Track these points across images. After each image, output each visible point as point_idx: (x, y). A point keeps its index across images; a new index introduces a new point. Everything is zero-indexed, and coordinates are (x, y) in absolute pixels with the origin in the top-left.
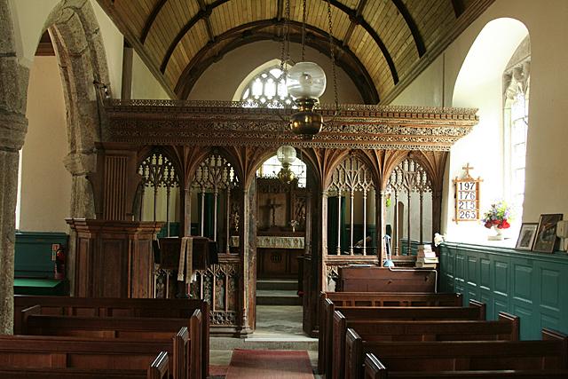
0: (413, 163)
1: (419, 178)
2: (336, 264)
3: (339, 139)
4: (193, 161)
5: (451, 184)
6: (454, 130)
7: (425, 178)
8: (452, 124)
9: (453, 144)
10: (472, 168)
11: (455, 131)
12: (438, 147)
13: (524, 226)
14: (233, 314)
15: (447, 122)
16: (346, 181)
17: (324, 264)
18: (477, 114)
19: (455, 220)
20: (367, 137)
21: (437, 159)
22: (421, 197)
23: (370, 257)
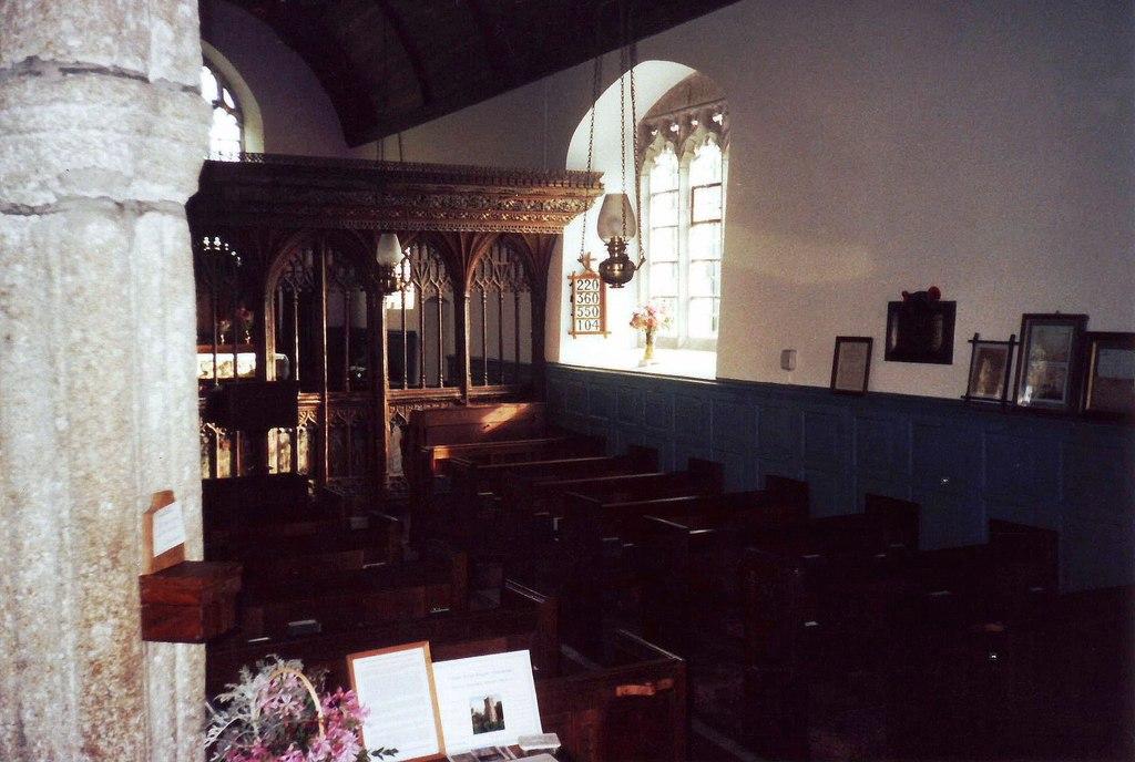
0: (505, 249)
1: (513, 272)
2: (404, 403)
3: (413, 216)
4: (474, 251)
5: (565, 284)
6: (572, 204)
7: (521, 272)
8: (571, 196)
9: (568, 223)
10: (593, 260)
11: (573, 205)
12: (545, 225)
13: (842, 345)
14: (359, 480)
15: (563, 192)
16: (494, 278)
17: (386, 403)
18: (602, 180)
19: (573, 333)
20: (453, 211)
21: (543, 243)
22: (517, 299)
23: (450, 390)
